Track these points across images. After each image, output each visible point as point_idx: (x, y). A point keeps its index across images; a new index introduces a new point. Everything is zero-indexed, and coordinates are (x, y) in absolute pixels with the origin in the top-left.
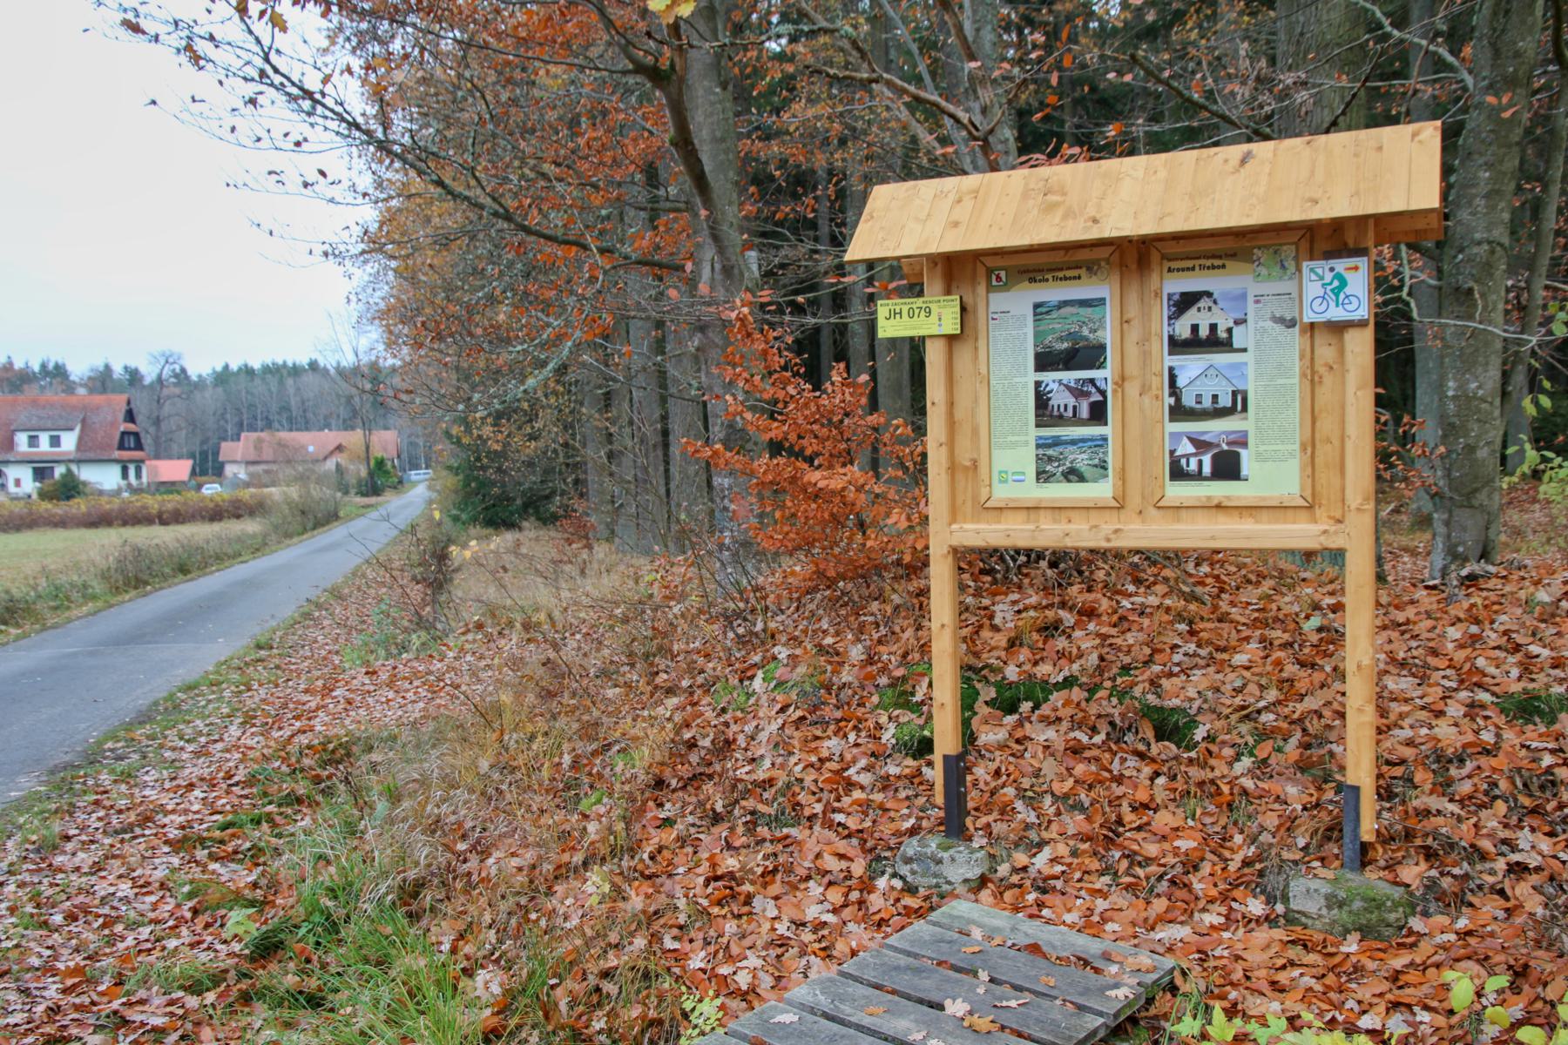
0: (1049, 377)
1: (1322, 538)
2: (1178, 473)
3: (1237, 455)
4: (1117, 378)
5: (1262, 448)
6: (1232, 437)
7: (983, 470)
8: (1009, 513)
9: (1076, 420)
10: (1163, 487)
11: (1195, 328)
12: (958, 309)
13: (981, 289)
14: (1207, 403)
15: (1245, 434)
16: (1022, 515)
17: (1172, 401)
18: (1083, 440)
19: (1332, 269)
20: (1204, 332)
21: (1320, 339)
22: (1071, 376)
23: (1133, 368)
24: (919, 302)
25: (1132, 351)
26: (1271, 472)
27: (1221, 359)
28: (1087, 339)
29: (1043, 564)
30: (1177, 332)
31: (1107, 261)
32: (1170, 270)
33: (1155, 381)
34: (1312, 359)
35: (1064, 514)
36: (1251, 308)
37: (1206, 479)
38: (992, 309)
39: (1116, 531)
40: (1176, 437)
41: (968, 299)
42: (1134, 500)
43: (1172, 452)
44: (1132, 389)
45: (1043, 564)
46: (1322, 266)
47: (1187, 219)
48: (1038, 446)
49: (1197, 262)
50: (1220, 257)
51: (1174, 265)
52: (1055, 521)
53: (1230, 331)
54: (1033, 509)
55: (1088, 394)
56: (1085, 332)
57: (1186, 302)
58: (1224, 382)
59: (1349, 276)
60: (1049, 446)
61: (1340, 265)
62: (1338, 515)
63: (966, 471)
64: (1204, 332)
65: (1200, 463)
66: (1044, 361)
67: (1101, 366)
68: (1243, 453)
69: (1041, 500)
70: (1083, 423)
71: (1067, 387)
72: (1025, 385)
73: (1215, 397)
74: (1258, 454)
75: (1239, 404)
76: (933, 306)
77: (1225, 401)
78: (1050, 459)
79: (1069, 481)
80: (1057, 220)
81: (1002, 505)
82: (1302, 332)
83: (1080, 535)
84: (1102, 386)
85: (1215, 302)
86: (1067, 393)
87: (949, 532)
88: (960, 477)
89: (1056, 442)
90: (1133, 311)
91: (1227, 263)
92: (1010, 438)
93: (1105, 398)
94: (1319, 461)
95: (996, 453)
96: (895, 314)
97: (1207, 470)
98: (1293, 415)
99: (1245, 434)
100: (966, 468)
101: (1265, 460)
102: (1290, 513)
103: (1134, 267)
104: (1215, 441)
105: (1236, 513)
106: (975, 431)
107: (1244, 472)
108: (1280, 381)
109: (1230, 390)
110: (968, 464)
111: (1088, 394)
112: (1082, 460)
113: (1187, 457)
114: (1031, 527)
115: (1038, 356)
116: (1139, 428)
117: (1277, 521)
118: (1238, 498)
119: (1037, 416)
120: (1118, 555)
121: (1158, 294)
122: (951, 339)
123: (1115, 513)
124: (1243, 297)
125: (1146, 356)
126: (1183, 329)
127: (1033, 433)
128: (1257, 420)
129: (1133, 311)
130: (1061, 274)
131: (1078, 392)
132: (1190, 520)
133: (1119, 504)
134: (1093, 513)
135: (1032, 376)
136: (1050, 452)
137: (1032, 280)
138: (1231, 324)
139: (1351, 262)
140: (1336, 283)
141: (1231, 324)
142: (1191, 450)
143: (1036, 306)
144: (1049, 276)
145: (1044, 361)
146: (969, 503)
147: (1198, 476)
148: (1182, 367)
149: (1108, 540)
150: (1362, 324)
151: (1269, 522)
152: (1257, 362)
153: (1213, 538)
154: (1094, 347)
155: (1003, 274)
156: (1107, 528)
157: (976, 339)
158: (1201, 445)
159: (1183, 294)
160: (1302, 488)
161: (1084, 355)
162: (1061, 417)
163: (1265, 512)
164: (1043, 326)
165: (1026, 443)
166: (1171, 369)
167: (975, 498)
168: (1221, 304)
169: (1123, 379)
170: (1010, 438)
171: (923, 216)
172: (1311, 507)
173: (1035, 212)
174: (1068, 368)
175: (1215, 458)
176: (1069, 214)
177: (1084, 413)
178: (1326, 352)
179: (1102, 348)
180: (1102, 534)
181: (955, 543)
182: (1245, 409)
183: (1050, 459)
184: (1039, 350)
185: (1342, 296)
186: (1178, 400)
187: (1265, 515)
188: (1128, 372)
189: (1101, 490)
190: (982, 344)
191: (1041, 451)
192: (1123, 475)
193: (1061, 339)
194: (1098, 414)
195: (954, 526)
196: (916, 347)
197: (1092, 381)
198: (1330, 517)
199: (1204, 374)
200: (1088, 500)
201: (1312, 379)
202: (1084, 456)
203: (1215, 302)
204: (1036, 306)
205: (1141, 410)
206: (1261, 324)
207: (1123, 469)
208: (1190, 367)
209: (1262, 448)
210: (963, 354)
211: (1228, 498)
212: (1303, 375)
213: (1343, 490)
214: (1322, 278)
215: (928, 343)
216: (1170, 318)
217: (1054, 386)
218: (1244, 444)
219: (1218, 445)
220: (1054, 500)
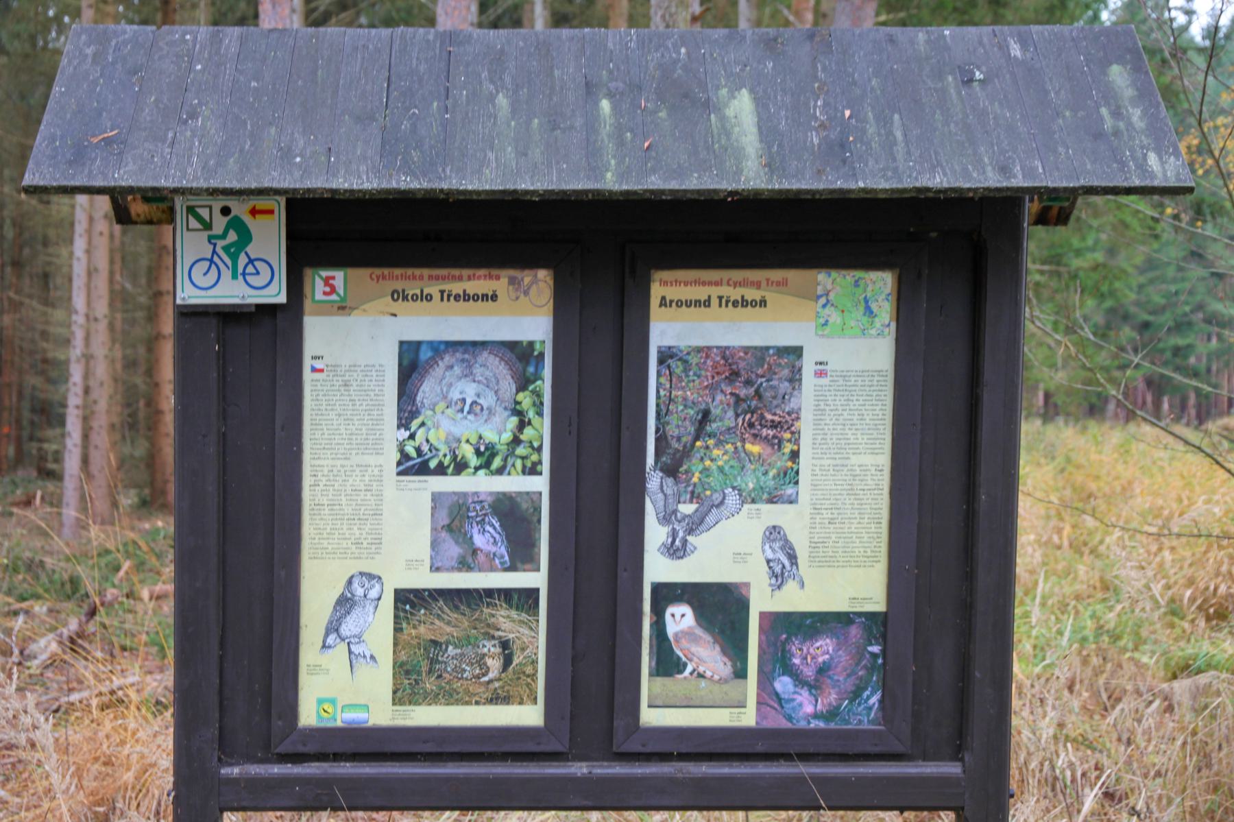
19: (226, 211)
91: (770, 296)
140: (232, 236)
185: (243, 260)
214: (208, 226)
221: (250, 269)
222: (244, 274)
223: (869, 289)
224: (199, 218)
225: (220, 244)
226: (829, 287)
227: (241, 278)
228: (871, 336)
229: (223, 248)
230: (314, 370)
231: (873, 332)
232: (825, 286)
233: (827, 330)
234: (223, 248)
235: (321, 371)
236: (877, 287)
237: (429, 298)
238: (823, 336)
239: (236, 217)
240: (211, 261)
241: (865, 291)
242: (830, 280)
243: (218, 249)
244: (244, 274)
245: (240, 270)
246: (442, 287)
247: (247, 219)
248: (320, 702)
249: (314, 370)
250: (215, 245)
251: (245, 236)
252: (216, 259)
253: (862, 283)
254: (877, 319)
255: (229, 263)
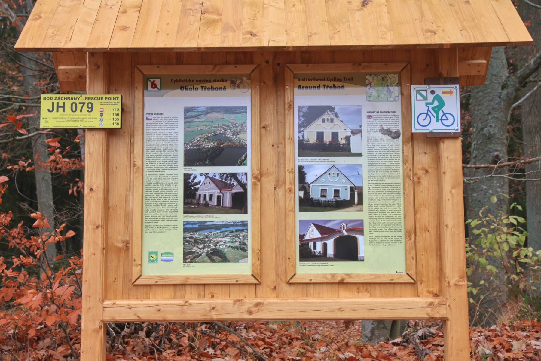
0: (197, 171)
1: (429, 310)
2: (307, 254)
3: (355, 240)
4: (256, 173)
5: (375, 234)
6: (350, 225)
7: (135, 250)
8: (158, 289)
9: (220, 208)
10: (294, 266)
11: (320, 135)
12: (119, 107)
13: (138, 94)
14: (330, 196)
15: (361, 222)
16: (170, 292)
17: (302, 194)
18: (226, 226)
19: (433, 92)
20: (327, 139)
21: (419, 148)
22: (216, 171)
23: (269, 165)
24: (82, 98)
25: (269, 152)
26: (382, 256)
27: (341, 161)
28: (230, 140)
29: (142, 334)
30: (306, 137)
31: (249, 77)
32: (300, 87)
33: (288, 177)
34: (413, 164)
35: (208, 290)
36: (365, 121)
37: (330, 259)
38: (147, 111)
39: (257, 305)
40: (304, 224)
41: (127, 102)
42: (270, 278)
43: (302, 237)
44: (268, 183)
45: (142, 334)
46: (425, 90)
47: (332, 38)
48: (186, 230)
49: (322, 83)
50: (340, 80)
51: (303, 83)
52: (199, 297)
53: (348, 139)
54: (179, 286)
55: (231, 186)
56: (229, 134)
57: (312, 114)
58: (344, 180)
59: (444, 97)
60: (195, 230)
61: (439, 89)
62: (436, 290)
63: (121, 252)
64: (327, 139)
65: (325, 246)
66: (193, 157)
67: (243, 163)
68: (360, 238)
69: (188, 278)
70: (226, 211)
71: (213, 179)
72: (175, 177)
73: (337, 192)
74: (372, 239)
75: (355, 198)
76: (96, 103)
77: (345, 196)
78: (196, 242)
79: (213, 261)
80: (218, 31)
81: (153, 282)
82: (405, 142)
83: (225, 307)
84: (244, 180)
85: (336, 115)
86: (213, 185)
87: (99, 309)
88: (112, 256)
89: (203, 227)
90: (270, 120)
91: (345, 84)
92: (161, 223)
93: (245, 189)
94: (420, 245)
95: (147, 236)
96: (56, 108)
97: (330, 251)
98: (398, 209)
99: (361, 222)
100: (119, 249)
101: (378, 244)
102: (398, 288)
103: (271, 83)
104: (337, 228)
105: (354, 288)
106: (129, 216)
107: (361, 254)
108: (388, 181)
109: (349, 186)
110: (120, 245)
111: (231, 186)
112: (224, 243)
113: (315, 240)
114: (181, 302)
115: (187, 153)
116: (273, 216)
117: (388, 296)
118: (358, 276)
119: (185, 204)
120: (192, 325)
121: (291, 106)
122: (110, 133)
123: (253, 288)
124: (358, 112)
125: (281, 156)
126: (310, 135)
127: (181, 218)
128: (371, 212)
129: (270, 120)
130: (209, 85)
131: (222, 184)
132: (318, 295)
133: (257, 282)
134: (233, 289)
135: (181, 170)
136: (197, 235)
137: (182, 88)
138: (349, 134)
139: (448, 87)
140: (436, 103)
141: (349, 134)
142: (318, 235)
143: (187, 110)
144: (199, 86)
145: (193, 157)
146: (120, 281)
147: (323, 257)
148: (310, 166)
149: (250, 313)
150: (453, 137)
151: (382, 296)
152: (369, 165)
153: (340, 310)
154: (236, 147)
155: (158, 82)
156: (250, 301)
157: (132, 136)
158: (325, 231)
159: (310, 107)
160: (407, 267)
161: (225, 152)
162: (207, 205)
163: (377, 287)
164: (193, 128)
165: (175, 228)
166: (301, 168)
167: (126, 277)
168: (341, 117)
169: (261, 174)
170: (161, 223)
171: (92, 20)
172: (413, 284)
173: (197, 24)
174: (213, 164)
175: (337, 243)
176: (227, 28)
177: (227, 202)
178: (423, 159)
179: (243, 148)
180: (245, 308)
181: (107, 318)
182: (361, 202)
183: (196, 242)
184: (189, 148)
185: (441, 114)
186: (307, 193)
187: (377, 290)
188: (265, 169)
189: (242, 269)
190: (137, 140)
191: (188, 235)
192: (260, 255)
193: (208, 139)
194: (239, 203)
195: (107, 303)
196: (69, 140)
197: (234, 176)
198: (429, 292)
199: (327, 172)
200: (231, 277)
201: (413, 179)
202: (226, 239)
203: (336, 115)
204: (187, 110)
205: (276, 201)
206: (372, 134)
207: (261, 251)
208: (317, 167)
209: (375, 234)
210: (120, 148)
211: (349, 275)
212: (406, 176)
213: (441, 270)
214: (425, 99)
215: (88, 135)
216: (300, 126)
217: (202, 179)
218: (361, 231)
219: (340, 232)
220: (199, 278)
221: (444, 118)
222: (441, 120)
223: (389, 81)
224: (422, 95)
225: (431, 106)
226: (371, 81)
227: (440, 121)
228: (391, 101)
229: (433, 109)
230: (148, 119)
231: (391, 99)
232: (369, 80)
233: (371, 99)
234: (433, 109)
235: (151, 119)
236: (392, 80)
237: (197, 88)
238: (369, 101)
239: (437, 95)
240: (427, 114)
241: (387, 82)
242: (371, 78)
243: (430, 109)
244: (441, 120)
245: (440, 118)
246: (202, 85)
247: (443, 96)
248: (150, 253)
249: (148, 119)
250: (429, 107)
251: (442, 104)
252: (429, 113)
253: (385, 79)
254: (393, 94)
255: (435, 115)
